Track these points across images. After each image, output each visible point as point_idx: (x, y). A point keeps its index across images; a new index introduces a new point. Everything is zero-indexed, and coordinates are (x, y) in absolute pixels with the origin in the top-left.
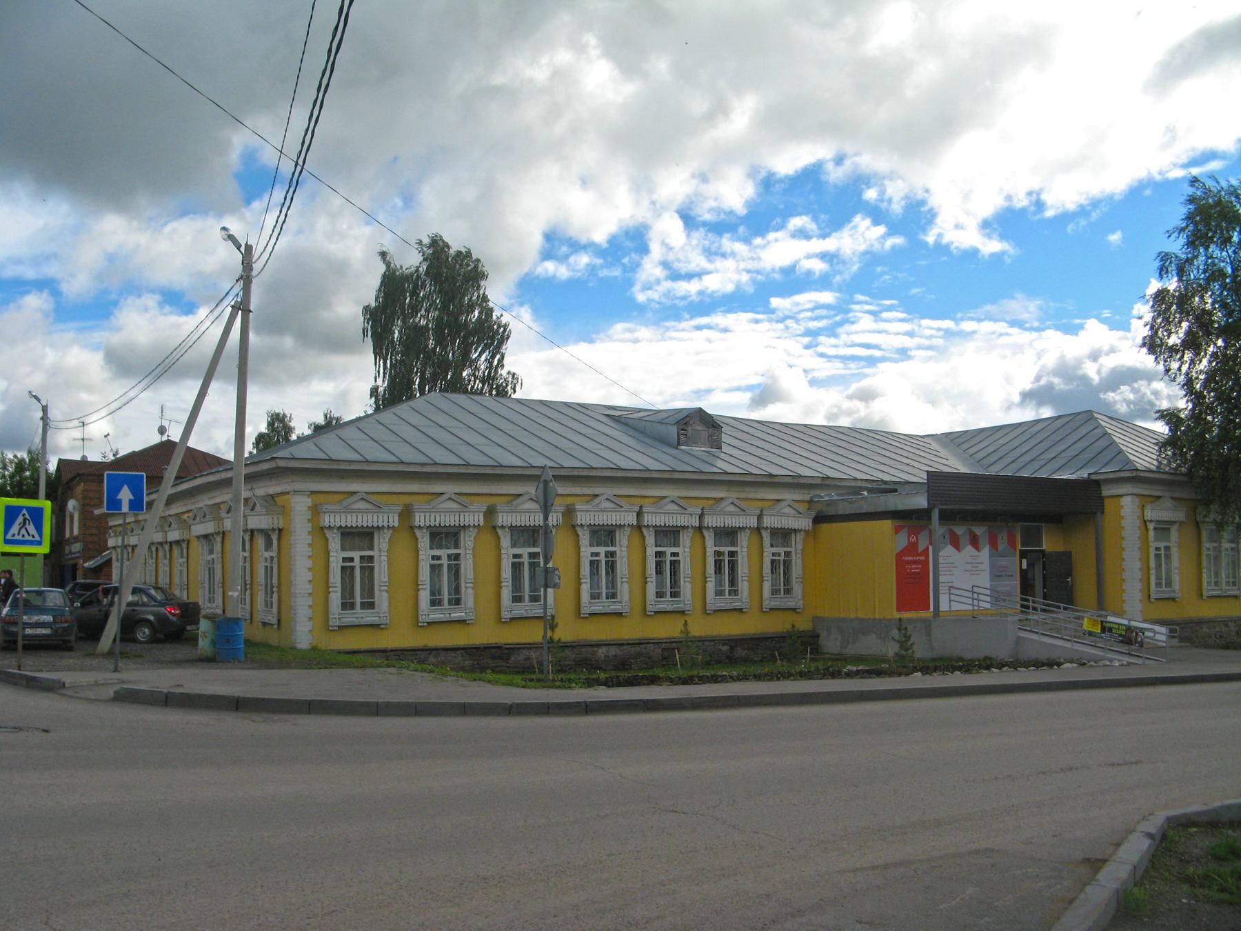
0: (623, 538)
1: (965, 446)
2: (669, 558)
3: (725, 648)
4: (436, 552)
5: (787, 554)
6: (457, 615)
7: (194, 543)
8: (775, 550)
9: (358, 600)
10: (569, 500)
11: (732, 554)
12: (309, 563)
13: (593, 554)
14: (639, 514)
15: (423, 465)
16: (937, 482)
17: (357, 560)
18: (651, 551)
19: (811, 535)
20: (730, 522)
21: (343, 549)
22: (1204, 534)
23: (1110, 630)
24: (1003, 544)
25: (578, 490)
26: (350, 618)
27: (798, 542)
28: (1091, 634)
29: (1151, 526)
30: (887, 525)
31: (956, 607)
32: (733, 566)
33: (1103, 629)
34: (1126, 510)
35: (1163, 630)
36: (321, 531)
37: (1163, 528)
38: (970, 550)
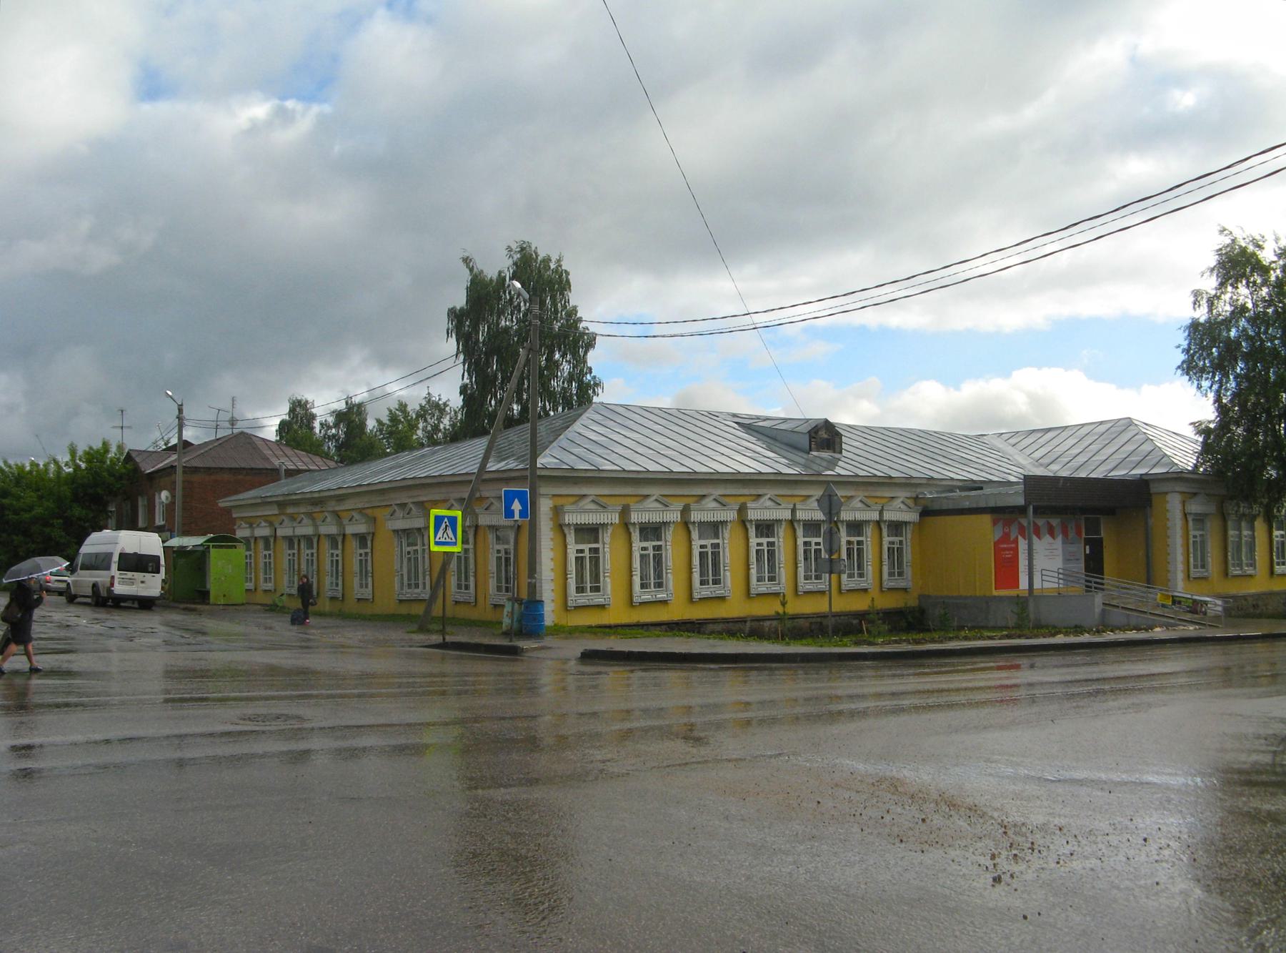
0: (669, 535)
1: (1028, 451)
2: (814, 547)
3: (855, 622)
4: (581, 547)
5: (770, 544)
6: (661, 596)
7: (349, 539)
8: (703, 542)
9: (711, 578)
10: (742, 500)
11: (859, 543)
12: (551, 554)
13: (578, 551)
14: (794, 511)
15: (638, 472)
16: (1033, 484)
17: (587, 551)
18: (800, 541)
19: (920, 525)
20: (860, 516)
21: (576, 542)
22: (1230, 524)
23: (1180, 603)
24: (1072, 534)
25: (746, 491)
26: (583, 600)
27: (908, 534)
28: (1163, 606)
29: (1190, 519)
30: (986, 519)
31: (1046, 585)
32: (860, 552)
33: (1174, 602)
34: (1173, 506)
35: (1219, 602)
36: (560, 528)
37: (1200, 519)
38: (1047, 538)
